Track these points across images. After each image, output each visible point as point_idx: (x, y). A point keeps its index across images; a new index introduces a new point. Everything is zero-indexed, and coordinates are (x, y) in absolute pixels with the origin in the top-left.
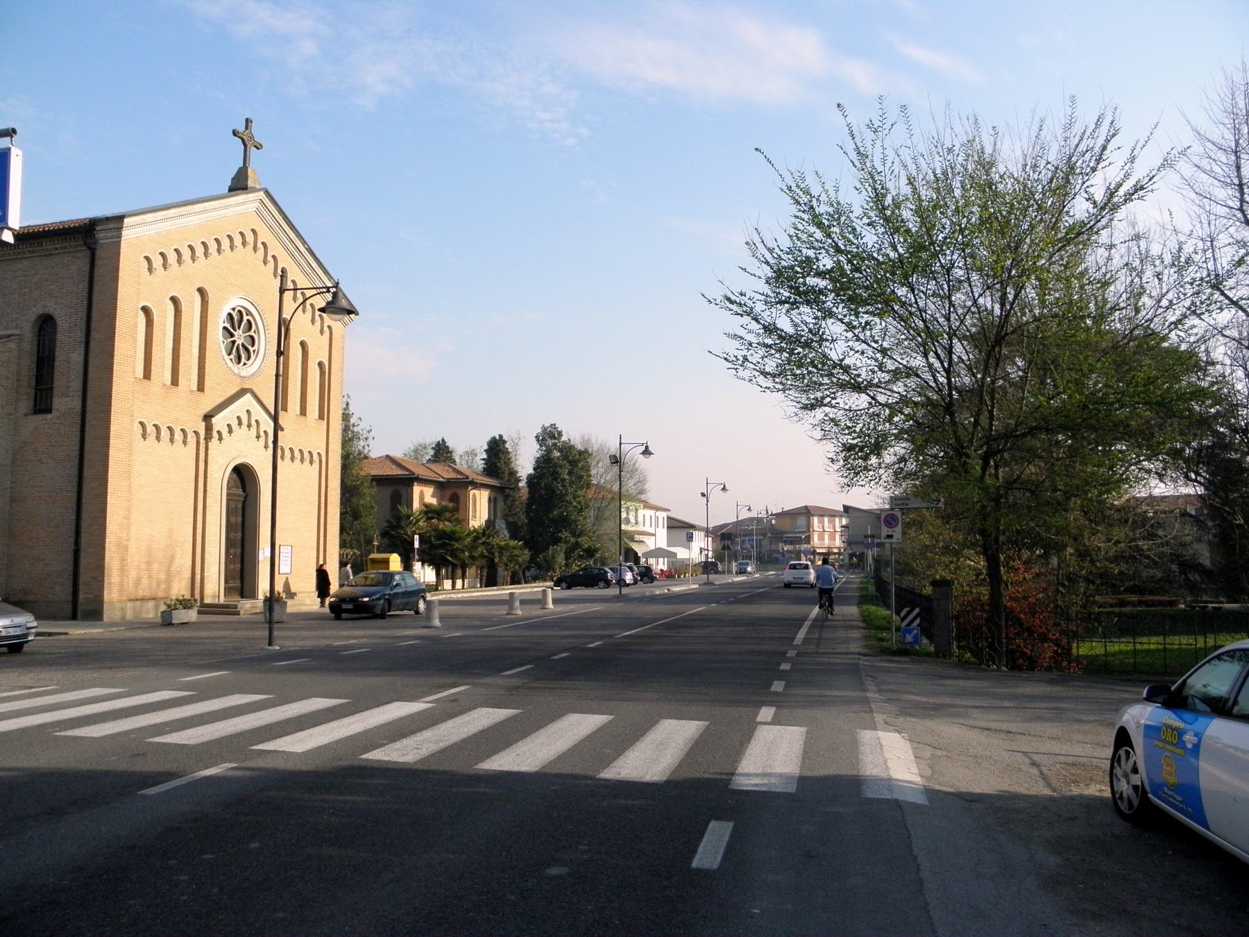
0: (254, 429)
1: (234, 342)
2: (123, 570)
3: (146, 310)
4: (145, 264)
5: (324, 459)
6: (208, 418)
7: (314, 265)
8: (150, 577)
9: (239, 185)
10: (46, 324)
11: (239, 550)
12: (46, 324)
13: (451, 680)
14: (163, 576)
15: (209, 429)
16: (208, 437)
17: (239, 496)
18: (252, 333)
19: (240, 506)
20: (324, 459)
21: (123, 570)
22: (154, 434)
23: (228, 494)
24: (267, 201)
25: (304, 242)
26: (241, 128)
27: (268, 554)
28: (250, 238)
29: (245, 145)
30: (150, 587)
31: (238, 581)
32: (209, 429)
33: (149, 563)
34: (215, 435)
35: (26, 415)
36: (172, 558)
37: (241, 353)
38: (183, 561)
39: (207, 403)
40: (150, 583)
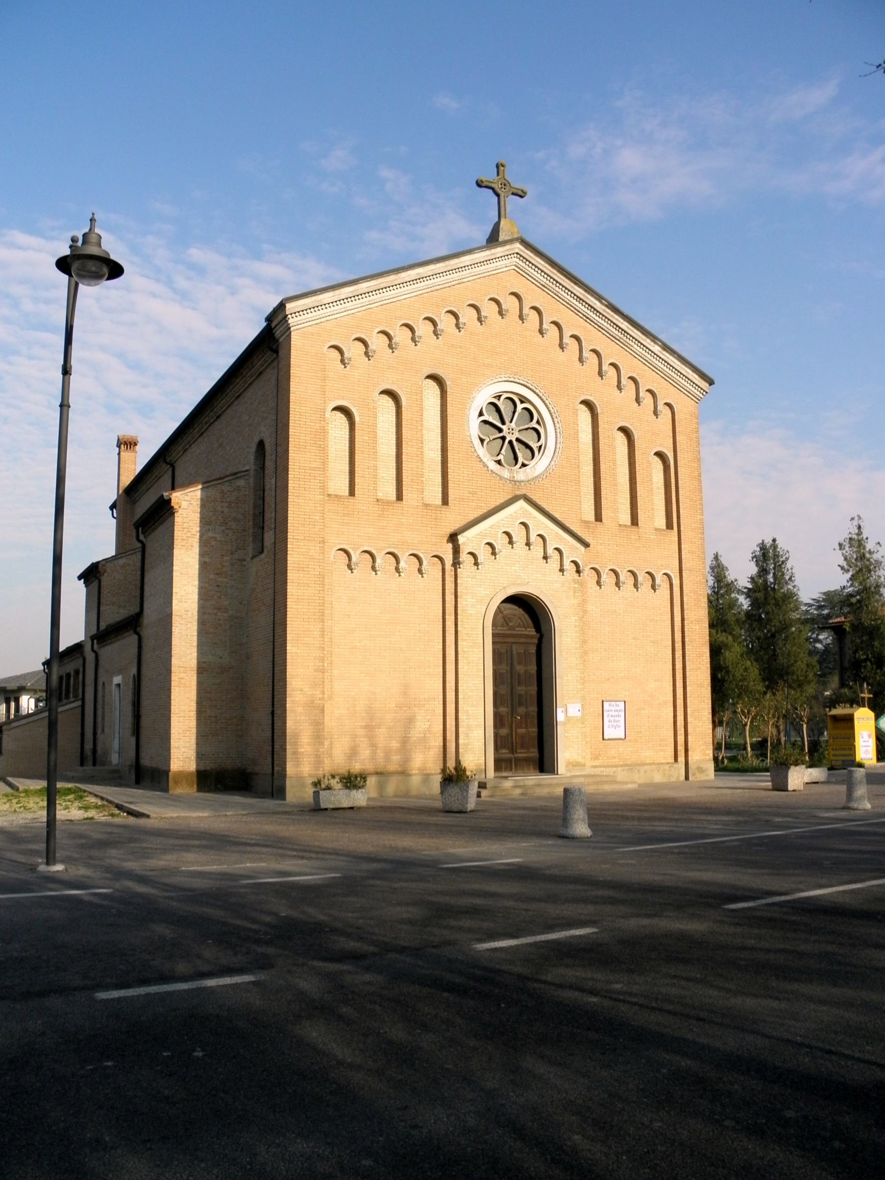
0: (537, 549)
1: (510, 442)
2: (318, 737)
3: (624, 430)
4: (336, 354)
5: (676, 582)
6: (453, 538)
7: (625, 325)
8: (373, 746)
9: (493, 239)
10: (261, 444)
11: (534, 709)
12: (261, 444)
13: (824, 881)
14: (395, 744)
15: (456, 551)
16: (456, 563)
17: (531, 637)
18: (534, 424)
19: (533, 649)
20: (676, 582)
21: (318, 737)
22: (631, 580)
23: (494, 635)
24: (528, 254)
25: (600, 298)
26: (489, 175)
27: (93, 677)
28: (510, 304)
29: (498, 195)
30: (373, 757)
31: (536, 750)
32: (456, 551)
33: (370, 728)
34: (464, 557)
35: (253, 557)
36: (410, 721)
37: (518, 451)
38: (428, 723)
39: (452, 520)
40: (374, 753)
